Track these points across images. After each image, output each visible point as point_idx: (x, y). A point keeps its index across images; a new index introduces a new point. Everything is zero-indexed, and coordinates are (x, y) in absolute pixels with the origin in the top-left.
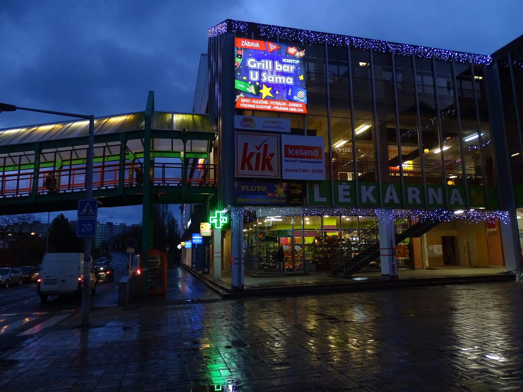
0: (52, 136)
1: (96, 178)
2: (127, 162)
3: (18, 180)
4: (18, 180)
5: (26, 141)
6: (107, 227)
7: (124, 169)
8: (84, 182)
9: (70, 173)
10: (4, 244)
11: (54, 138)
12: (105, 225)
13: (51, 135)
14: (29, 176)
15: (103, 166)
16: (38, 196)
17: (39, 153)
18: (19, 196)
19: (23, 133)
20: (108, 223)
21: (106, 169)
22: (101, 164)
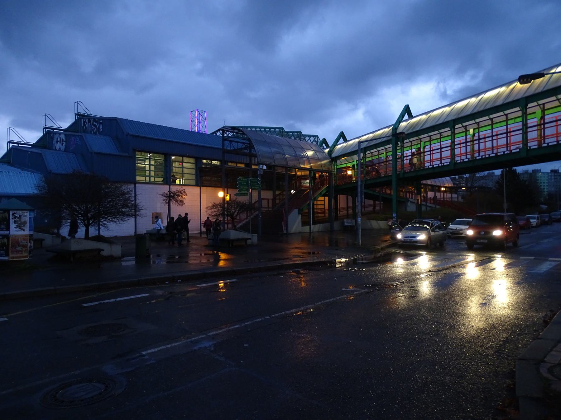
0: (537, 89)
1: (533, 135)
2: (456, 143)
3: (441, 152)
4: (441, 152)
5: (510, 100)
6: (551, 176)
7: (454, 149)
8: (521, 140)
9: (507, 135)
10: (458, 198)
11: (540, 90)
12: (548, 173)
13: (535, 87)
14: (536, 128)
15: (441, 148)
16: (456, 164)
17: (453, 128)
18: (487, 156)
19: (503, 93)
20: (552, 171)
21: (443, 150)
22: (491, 135)
